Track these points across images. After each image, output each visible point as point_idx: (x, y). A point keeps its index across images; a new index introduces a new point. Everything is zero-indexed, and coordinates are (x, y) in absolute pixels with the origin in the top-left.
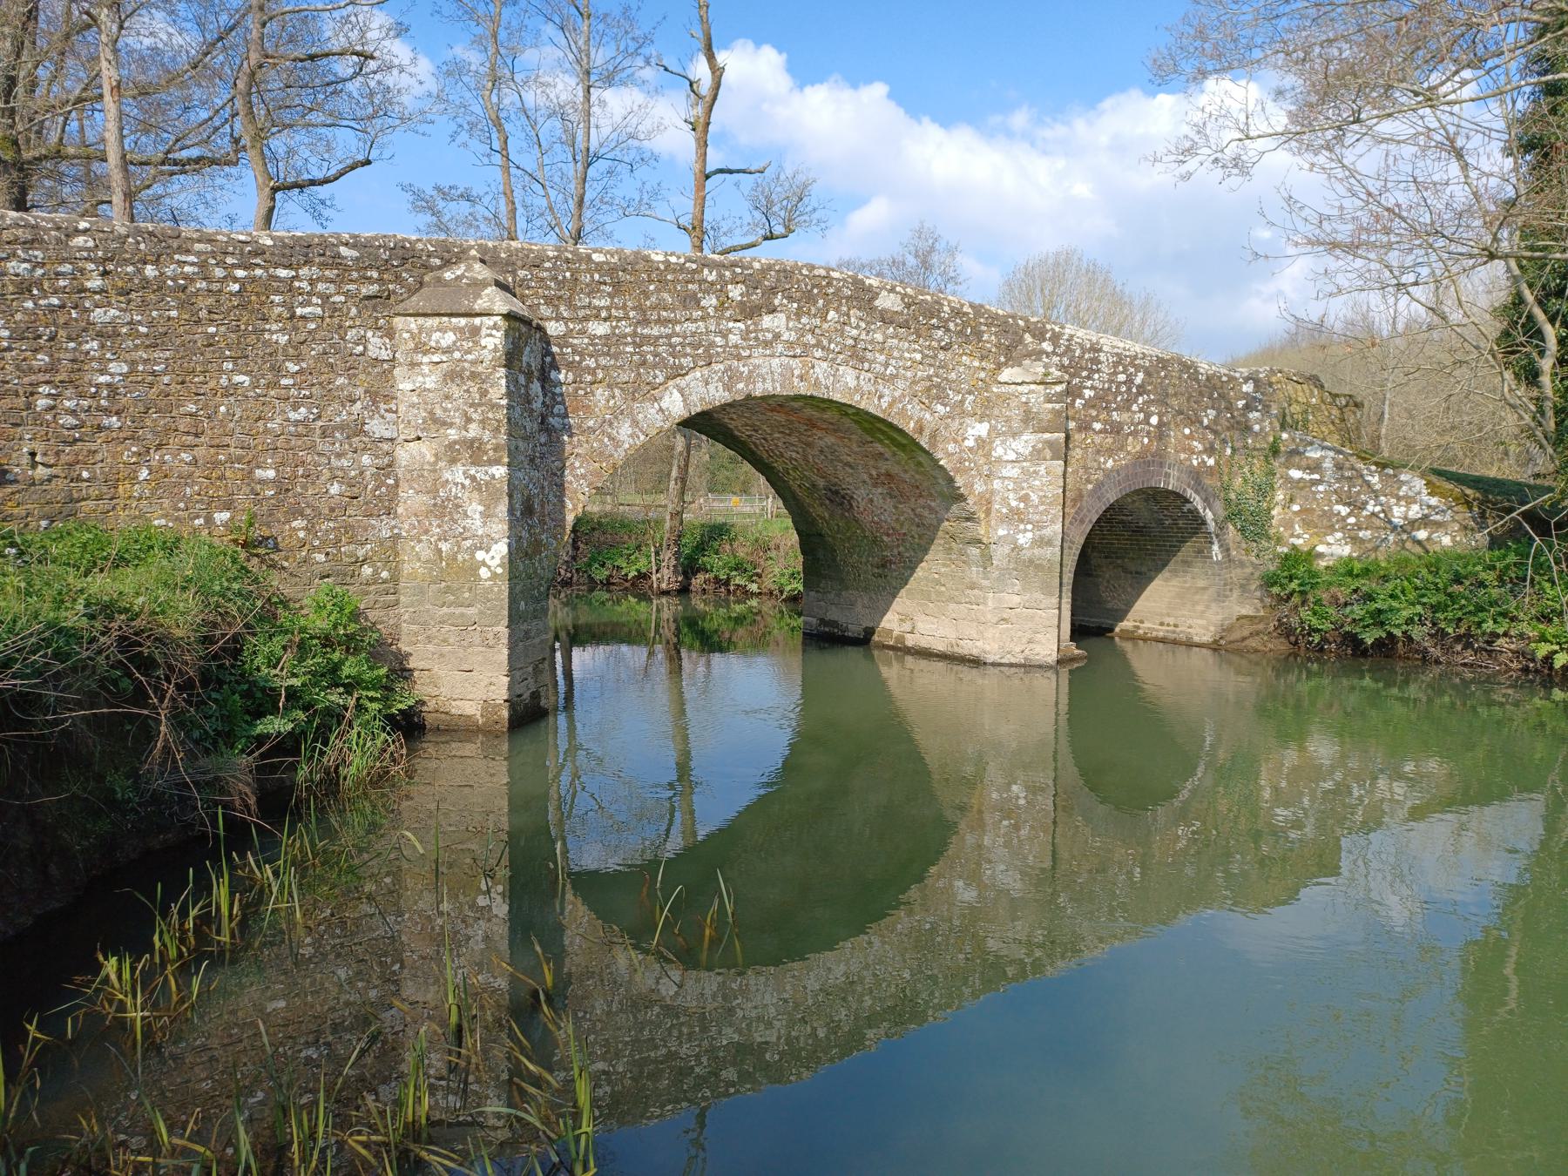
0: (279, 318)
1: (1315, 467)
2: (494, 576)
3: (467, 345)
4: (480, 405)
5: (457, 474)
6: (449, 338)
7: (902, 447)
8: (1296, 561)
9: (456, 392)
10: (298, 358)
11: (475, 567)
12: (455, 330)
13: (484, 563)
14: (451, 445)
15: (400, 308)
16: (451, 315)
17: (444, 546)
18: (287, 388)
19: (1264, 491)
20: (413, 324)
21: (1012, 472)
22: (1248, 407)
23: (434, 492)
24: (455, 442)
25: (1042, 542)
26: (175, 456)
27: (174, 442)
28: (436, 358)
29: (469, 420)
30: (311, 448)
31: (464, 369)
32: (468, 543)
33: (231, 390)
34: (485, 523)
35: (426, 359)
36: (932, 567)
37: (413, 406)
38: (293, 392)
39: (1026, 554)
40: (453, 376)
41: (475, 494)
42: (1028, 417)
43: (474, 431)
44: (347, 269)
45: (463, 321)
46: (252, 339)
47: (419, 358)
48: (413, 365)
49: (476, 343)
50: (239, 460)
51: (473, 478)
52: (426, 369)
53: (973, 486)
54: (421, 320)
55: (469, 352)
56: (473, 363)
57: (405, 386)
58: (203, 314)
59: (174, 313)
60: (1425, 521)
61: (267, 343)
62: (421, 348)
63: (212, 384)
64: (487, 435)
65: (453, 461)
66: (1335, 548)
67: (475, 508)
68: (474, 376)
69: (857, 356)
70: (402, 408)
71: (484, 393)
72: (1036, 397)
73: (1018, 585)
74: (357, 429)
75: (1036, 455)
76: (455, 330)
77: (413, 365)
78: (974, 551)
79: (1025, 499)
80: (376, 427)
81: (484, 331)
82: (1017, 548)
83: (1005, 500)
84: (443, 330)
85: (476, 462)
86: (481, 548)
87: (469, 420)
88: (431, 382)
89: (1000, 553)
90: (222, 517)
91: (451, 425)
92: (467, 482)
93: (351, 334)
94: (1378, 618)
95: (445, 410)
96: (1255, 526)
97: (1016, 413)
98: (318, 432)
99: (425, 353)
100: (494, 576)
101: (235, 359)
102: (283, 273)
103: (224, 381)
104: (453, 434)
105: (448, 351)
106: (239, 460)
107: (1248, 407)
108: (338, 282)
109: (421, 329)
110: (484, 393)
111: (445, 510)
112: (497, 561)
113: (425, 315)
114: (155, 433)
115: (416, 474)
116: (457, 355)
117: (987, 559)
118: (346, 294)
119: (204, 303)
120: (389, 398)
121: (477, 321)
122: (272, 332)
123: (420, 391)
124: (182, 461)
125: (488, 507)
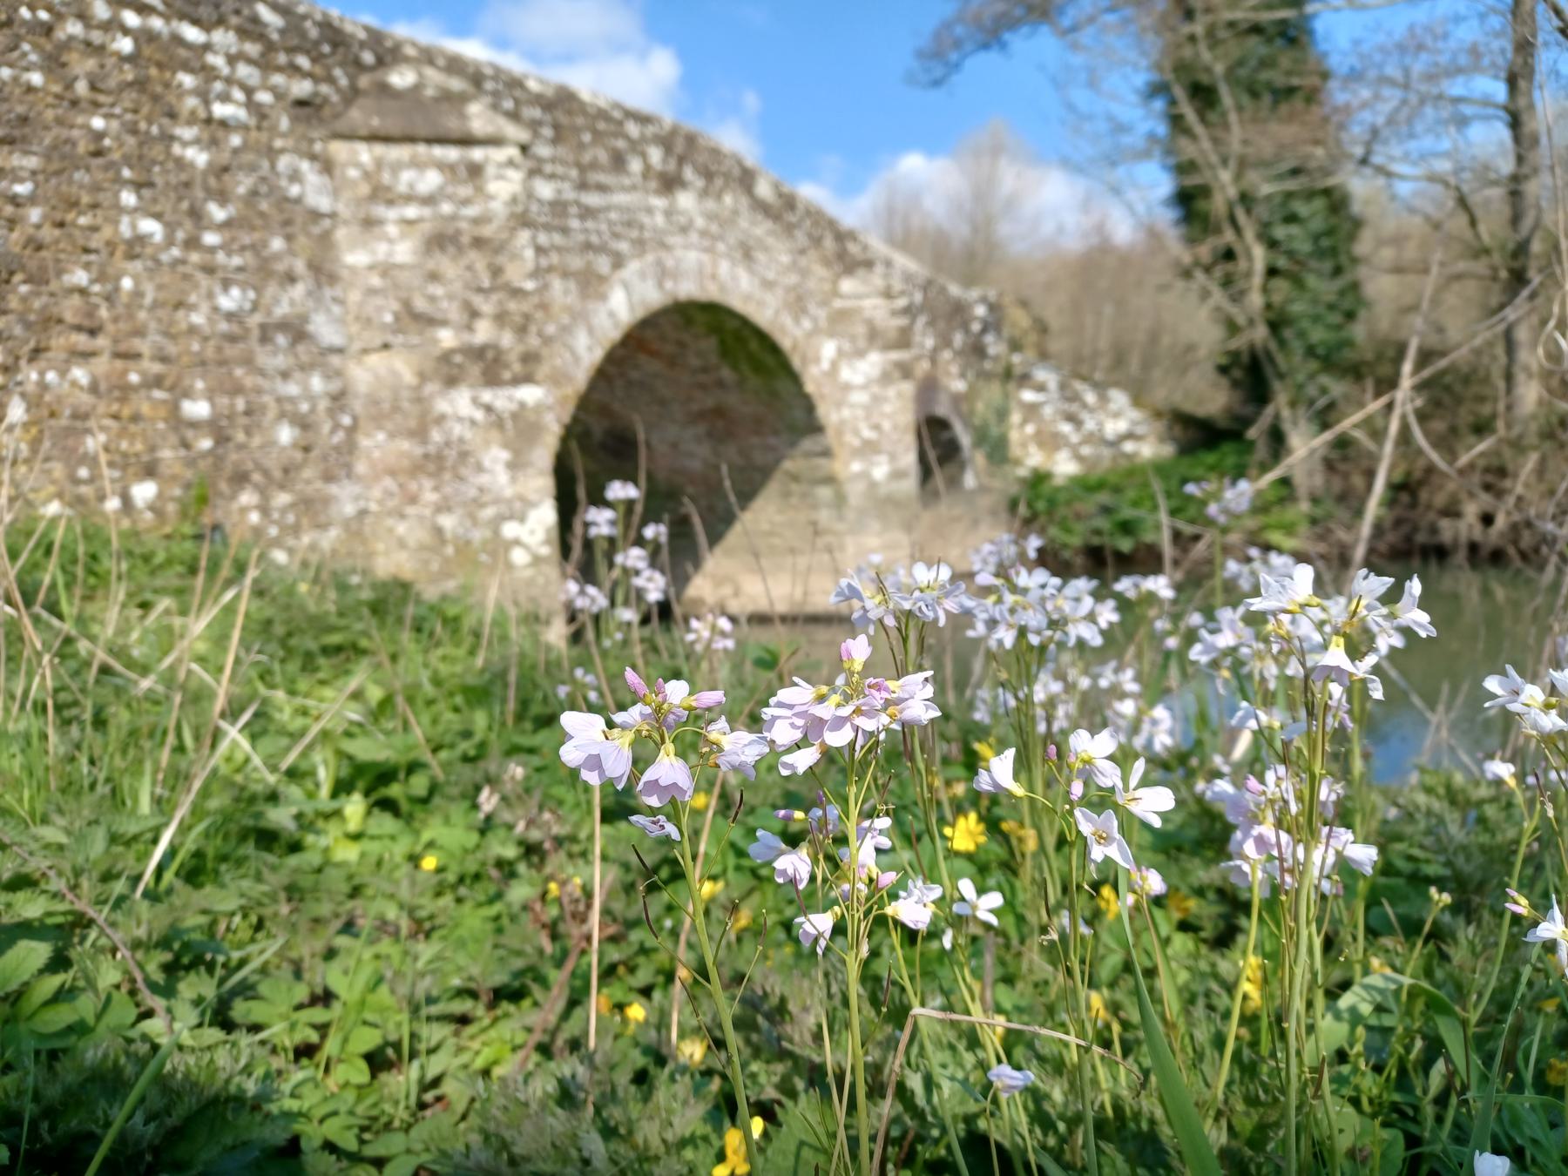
0: (192, 120)
1: (1041, 388)
2: (537, 560)
3: (465, 191)
4: (492, 290)
5: (460, 403)
6: (431, 180)
7: (759, 368)
8: (1039, 478)
9: (448, 266)
10: (223, 198)
11: (500, 548)
12: (442, 166)
13: (517, 542)
14: (446, 357)
15: (341, 125)
16: (430, 141)
17: (448, 522)
18: (212, 250)
19: (1002, 415)
20: (365, 154)
21: (860, 397)
22: (984, 330)
23: (420, 433)
24: (452, 351)
25: (897, 475)
26: (63, 373)
27: (60, 341)
28: (411, 212)
29: (474, 314)
30: (248, 361)
31: (458, 233)
32: (489, 512)
33: (136, 246)
34: (513, 480)
35: (391, 214)
36: (762, 516)
37: (372, 292)
38: (221, 257)
39: (883, 491)
40: (441, 241)
41: (495, 435)
42: (874, 336)
43: (483, 332)
44: (270, 47)
45: (452, 154)
46: (156, 151)
47: (380, 211)
48: (370, 223)
49: (480, 190)
50: (158, 382)
51: (489, 409)
52: (392, 230)
53: (828, 413)
54: (379, 149)
55: (466, 202)
56: (476, 221)
57: (355, 258)
58: (81, 88)
59: (36, 78)
60: (1130, 436)
61: (181, 163)
62: (381, 194)
63: (107, 232)
64: (507, 339)
65: (451, 382)
66: (1065, 467)
67: (496, 457)
68: (478, 243)
69: (746, 253)
70: (354, 297)
71: (496, 272)
72: (876, 309)
73: (875, 525)
74: (297, 331)
75: (885, 378)
76: (442, 166)
77: (370, 223)
78: (824, 492)
79: (877, 427)
80: (325, 329)
81: (491, 170)
82: (873, 485)
83: (856, 432)
84: (417, 164)
85: (492, 379)
86: (511, 517)
87: (474, 314)
88: (404, 251)
89: (855, 492)
90: (144, 492)
91: (444, 323)
92: (479, 415)
93: (284, 163)
94: (1126, 528)
95: (432, 299)
96: (998, 452)
97: (860, 330)
98: (256, 333)
99: (390, 203)
100: (537, 560)
101: (138, 186)
102: (192, 34)
103: (125, 229)
104: (447, 338)
105: (429, 200)
106: (158, 382)
107: (984, 330)
108: (264, 65)
109: (379, 163)
110: (496, 272)
111: (444, 464)
112: (540, 535)
113: (387, 139)
114: (28, 326)
115: (382, 412)
116: (446, 208)
117: (840, 500)
118: (273, 90)
119: (82, 66)
120: (333, 279)
121: (477, 154)
122: (185, 144)
123: (386, 269)
124: (74, 384)
125: (517, 453)
